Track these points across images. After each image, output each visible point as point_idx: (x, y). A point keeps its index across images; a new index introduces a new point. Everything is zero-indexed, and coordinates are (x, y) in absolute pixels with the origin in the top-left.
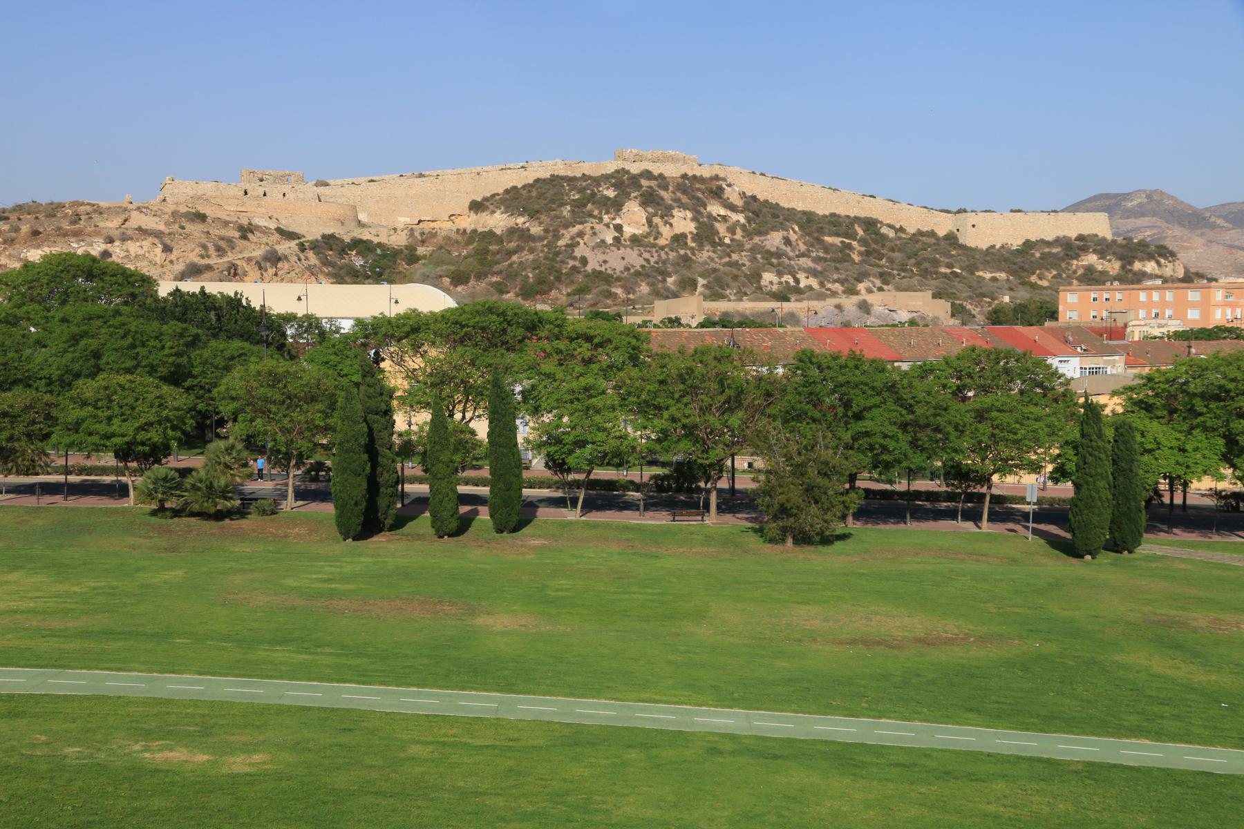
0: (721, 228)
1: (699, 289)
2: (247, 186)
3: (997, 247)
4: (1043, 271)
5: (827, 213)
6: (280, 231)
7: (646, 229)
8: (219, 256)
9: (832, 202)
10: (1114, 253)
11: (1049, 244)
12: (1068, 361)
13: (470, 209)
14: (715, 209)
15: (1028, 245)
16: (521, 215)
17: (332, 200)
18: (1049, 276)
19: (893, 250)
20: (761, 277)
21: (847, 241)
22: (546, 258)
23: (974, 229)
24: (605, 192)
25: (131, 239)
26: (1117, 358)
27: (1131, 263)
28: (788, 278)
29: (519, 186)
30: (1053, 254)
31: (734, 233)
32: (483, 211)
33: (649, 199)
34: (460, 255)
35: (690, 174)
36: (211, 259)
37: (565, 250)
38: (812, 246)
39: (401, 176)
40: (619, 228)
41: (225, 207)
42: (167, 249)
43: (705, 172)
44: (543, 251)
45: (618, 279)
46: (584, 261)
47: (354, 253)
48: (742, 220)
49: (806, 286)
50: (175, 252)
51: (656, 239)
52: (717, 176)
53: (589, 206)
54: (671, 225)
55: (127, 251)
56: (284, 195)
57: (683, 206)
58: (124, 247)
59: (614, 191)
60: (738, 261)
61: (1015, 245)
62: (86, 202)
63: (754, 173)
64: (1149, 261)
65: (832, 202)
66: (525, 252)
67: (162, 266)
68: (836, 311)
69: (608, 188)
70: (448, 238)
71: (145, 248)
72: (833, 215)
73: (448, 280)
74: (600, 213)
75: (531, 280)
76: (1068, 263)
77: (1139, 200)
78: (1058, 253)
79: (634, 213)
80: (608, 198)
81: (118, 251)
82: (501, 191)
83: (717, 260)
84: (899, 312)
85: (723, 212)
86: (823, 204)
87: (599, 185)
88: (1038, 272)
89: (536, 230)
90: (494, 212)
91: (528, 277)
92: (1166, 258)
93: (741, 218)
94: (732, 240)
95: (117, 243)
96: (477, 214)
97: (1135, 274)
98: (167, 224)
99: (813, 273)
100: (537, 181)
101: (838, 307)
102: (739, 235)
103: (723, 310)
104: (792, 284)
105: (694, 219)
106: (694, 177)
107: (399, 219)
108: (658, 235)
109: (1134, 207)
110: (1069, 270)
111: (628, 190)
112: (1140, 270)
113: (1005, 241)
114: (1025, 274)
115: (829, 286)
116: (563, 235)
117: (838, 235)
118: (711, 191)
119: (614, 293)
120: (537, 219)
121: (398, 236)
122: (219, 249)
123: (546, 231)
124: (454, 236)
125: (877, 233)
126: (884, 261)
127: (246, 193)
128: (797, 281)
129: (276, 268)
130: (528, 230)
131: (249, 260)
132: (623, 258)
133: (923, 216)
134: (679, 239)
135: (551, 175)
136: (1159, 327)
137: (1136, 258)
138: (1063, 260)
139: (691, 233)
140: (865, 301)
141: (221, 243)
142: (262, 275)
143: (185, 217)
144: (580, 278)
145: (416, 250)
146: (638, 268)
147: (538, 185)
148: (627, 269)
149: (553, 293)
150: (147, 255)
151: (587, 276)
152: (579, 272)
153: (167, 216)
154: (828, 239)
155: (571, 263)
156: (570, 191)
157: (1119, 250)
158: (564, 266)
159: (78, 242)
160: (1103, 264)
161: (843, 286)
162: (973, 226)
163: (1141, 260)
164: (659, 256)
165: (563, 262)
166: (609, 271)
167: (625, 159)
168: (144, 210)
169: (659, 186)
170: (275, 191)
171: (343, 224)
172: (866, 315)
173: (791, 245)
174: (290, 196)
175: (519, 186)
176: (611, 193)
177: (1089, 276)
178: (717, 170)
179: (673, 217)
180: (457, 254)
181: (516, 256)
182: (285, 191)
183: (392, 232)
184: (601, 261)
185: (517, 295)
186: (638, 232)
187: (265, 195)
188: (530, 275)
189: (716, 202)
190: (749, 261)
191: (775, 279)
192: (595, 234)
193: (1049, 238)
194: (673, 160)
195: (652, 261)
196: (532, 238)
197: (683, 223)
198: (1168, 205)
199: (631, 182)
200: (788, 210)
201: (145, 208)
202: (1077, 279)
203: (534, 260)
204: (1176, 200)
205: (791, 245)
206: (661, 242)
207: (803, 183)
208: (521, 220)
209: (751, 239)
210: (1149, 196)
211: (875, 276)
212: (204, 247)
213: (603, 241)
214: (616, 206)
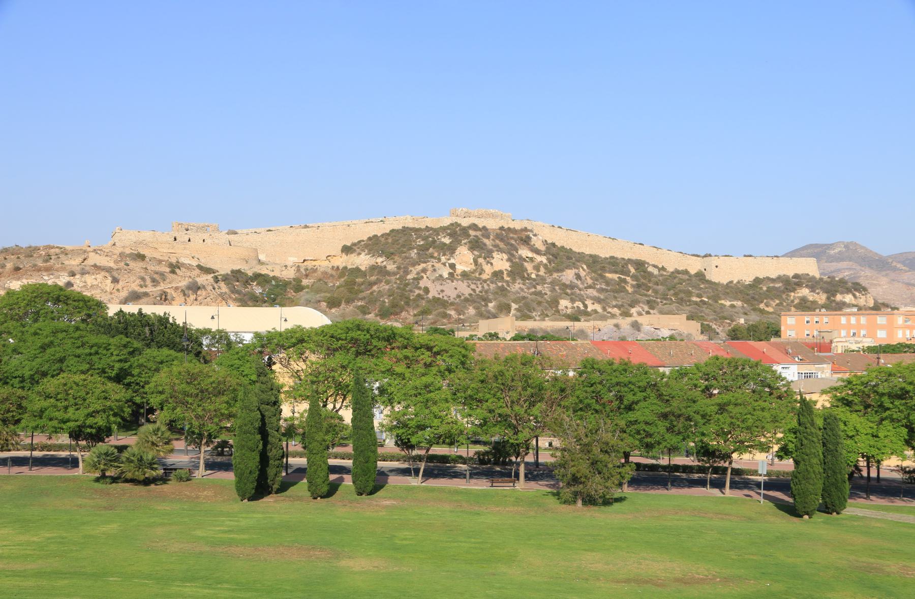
0: (529, 267)
1: (513, 312)
2: (176, 235)
3: (735, 282)
5: (608, 256)
6: (200, 267)
7: (473, 267)
9: (611, 248)
11: (773, 280)
12: (788, 368)
13: (342, 251)
14: (524, 252)
15: (757, 281)
16: (380, 256)
17: (239, 244)
18: (774, 304)
20: (558, 303)
21: (623, 277)
23: (717, 269)
24: (443, 240)
25: (89, 273)
26: (825, 366)
27: (834, 295)
30: (776, 288)
32: (352, 253)
33: (475, 245)
34: (334, 285)
37: (413, 282)
38: (597, 280)
39: (291, 227)
40: (453, 266)
41: (160, 250)
42: (115, 281)
43: (517, 226)
46: (427, 290)
47: (255, 283)
50: (121, 283)
51: (480, 274)
52: (526, 228)
54: (492, 264)
55: (85, 282)
56: (204, 241)
57: (501, 250)
58: (83, 279)
59: (449, 239)
61: (747, 281)
62: (55, 245)
63: (553, 226)
64: (848, 294)
65: (611, 248)
66: (383, 283)
67: (111, 293)
68: (615, 329)
70: (325, 273)
71: (99, 280)
72: (612, 257)
73: (325, 304)
75: (387, 304)
76: (787, 295)
77: (839, 249)
78: (779, 287)
79: (464, 255)
80: (445, 244)
82: (365, 239)
83: (526, 290)
84: (662, 330)
85: (530, 255)
87: (438, 235)
88: (765, 301)
89: (391, 267)
90: (359, 254)
91: (385, 302)
92: (860, 292)
93: (544, 259)
94: (537, 275)
95: (78, 276)
97: (837, 303)
98: (116, 262)
99: (598, 300)
101: (617, 326)
102: (542, 272)
104: (582, 308)
105: (509, 260)
106: (509, 229)
107: (289, 258)
108: (482, 271)
110: (788, 300)
112: (841, 301)
115: (610, 310)
116: (411, 271)
117: (616, 272)
120: (392, 259)
124: (330, 271)
127: (175, 239)
128: (586, 306)
129: (196, 295)
132: (456, 289)
133: (679, 259)
134: (497, 275)
135: (403, 227)
136: (856, 343)
140: (636, 322)
144: (424, 303)
145: (301, 281)
146: (467, 296)
148: (459, 296)
149: (403, 314)
150: (100, 285)
151: (429, 301)
152: (423, 299)
155: (417, 292)
156: (417, 238)
158: (412, 294)
159: (48, 275)
161: (620, 310)
162: (717, 267)
163: (842, 293)
165: (411, 291)
166: (445, 298)
168: (99, 252)
169: (483, 235)
170: (197, 238)
171: (247, 262)
172: (637, 332)
174: (208, 241)
176: (447, 240)
177: (803, 305)
178: (526, 224)
179: (493, 258)
180: (332, 284)
182: (204, 238)
184: (439, 290)
185: (377, 316)
187: (189, 241)
188: (386, 301)
191: (569, 305)
192: (435, 270)
193: (773, 276)
195: (478, 290)
196: (388, 273)
197: (500, 262)
199: (461, 232)
201: (100, 250)
202: (794, 306)
204: (867, 250)
207: (590, 234)
209: (551, 275)
210: (847, 246)
211: (644, 303)
212: (143, 279)
213: (441, 276)
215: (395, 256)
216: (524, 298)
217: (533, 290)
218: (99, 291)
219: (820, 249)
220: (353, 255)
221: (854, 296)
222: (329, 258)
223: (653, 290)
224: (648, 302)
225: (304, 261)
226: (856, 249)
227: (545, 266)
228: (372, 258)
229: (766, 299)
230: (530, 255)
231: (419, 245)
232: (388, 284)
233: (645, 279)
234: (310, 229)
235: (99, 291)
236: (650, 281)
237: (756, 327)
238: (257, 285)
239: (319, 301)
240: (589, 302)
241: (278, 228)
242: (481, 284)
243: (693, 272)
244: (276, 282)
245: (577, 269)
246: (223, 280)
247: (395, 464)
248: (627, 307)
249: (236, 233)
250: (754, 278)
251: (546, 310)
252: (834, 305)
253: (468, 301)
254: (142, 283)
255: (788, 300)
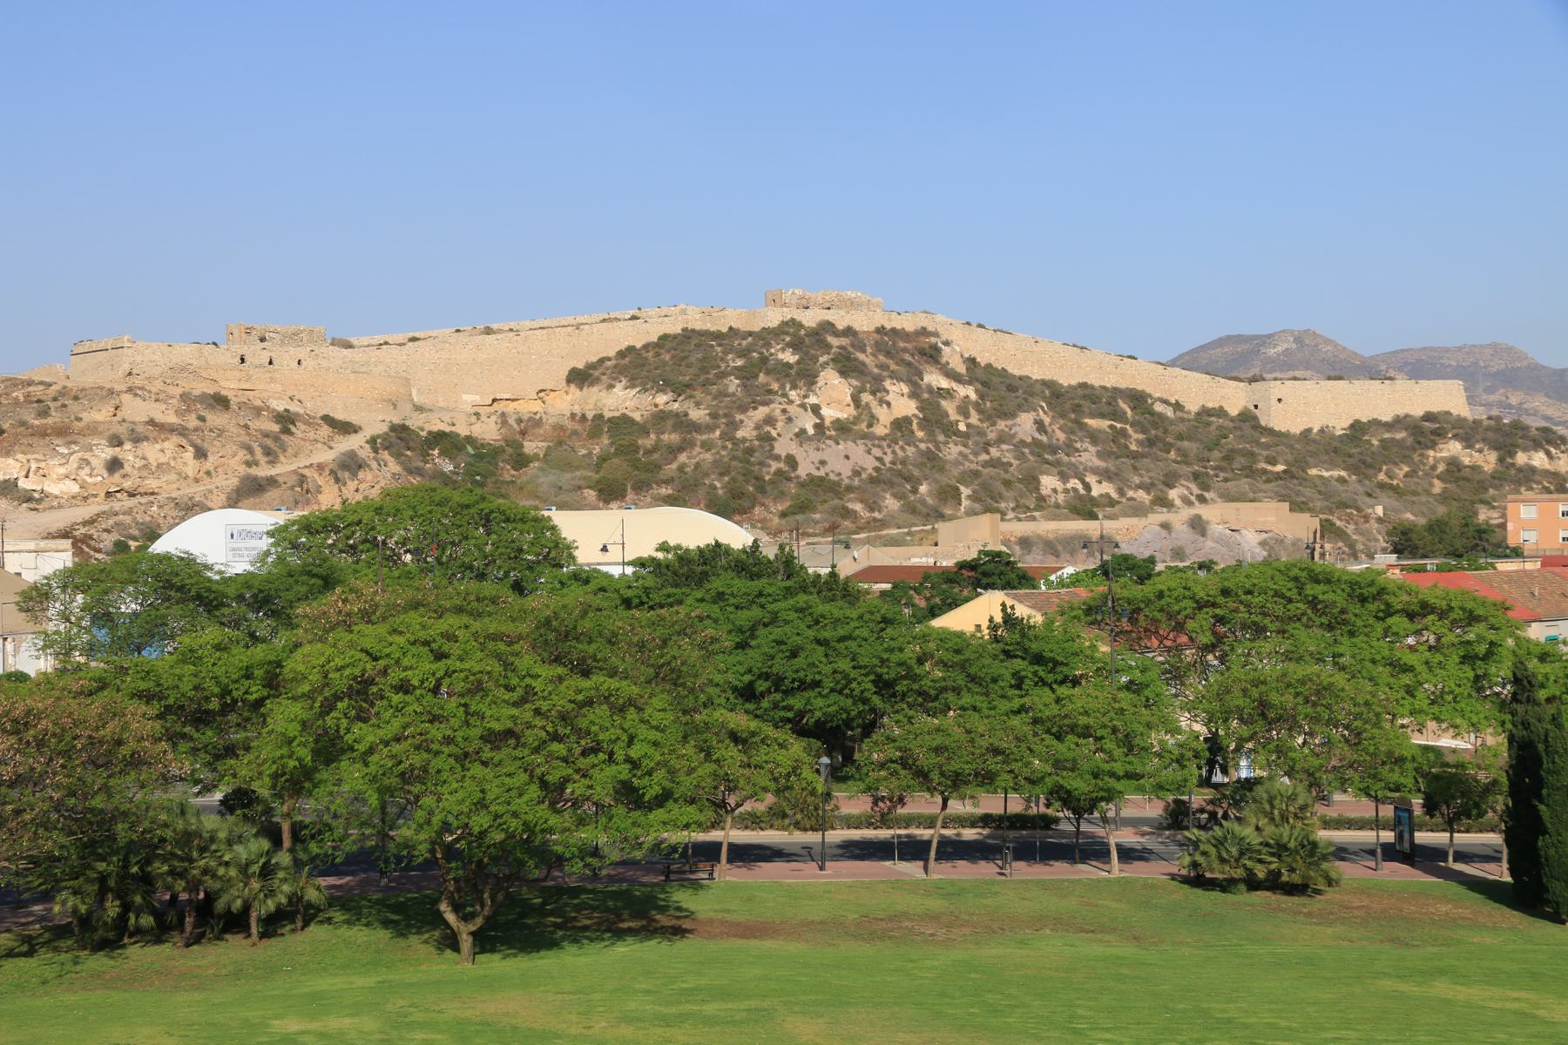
0: (949, 407)
1: (965, 503)
2: (245, 350)
3: (1315, 431)
4: (1391, 466)
5: (1074, 383)
6: (328, 420)
8: (270, 462)
9: (1079, 367)
10: (1484, 440)
11: (1388, 426)
13: (569, 381)
14: (934, 379)
15: (1357, 428)
16: (661, 390)
17: (363, 369)
18: (1401, 474)
19: (1180, 437)
20: (1039, 482)
21: (1119, 426)
22: (734, 458)
23: (1280, 405)
24: (780, 356)
25: (146, 439)
27: (1512, 454)
28: (1074, 483)
29: (638, 346)
30: (1398, 441)
31: (966, 415)
32: (591, 385)
33: (847, 366)
34: (590, 453)
35: (888, 327)
36: (260, 468)
37: (761, 446)
38: (1073, 432)
39: (458, 331)
40: (816, 409)
42: (201, 454)
43: (908, 323)
44: (724, 447)
45: (849, 489)
46: (792, 461)
47: (436, 452)
48: (973, 396)
49: (1101, 495)
50: (211, 458)
51: (870, 425)
52: (924, 329)
53: (762, 378)
54: (889, 404)
55: (144, 458)
56: (299, 362)
57: (895, 376)
58: (139, 453)
59: (793, 354)
60: (999, 458)
61: (1338, 428)
62: (37, 378)
63: (968, 324)
64: (1536, 450)
65: (1079, 367)
66: (698, 449)
68: (1164, 533)
69: (783, 350)
70: (559, 428)
72: (1083, 386)
73: (592, 493)
74: (783, 387)
75: (720, 492)
76: (1422, 455)
77: (1286, 346)
78: (1403, 440)
80: (788, 365)
81: (131, 458)
82: (612, 354)
83: (971, 457)
84: (1244, 532)
85: (944, 383)
86: (1069, 371)
87: (768, 345)
88: (1384, 468)
89: (697, 414)
90: (611, 387)
91: (715, 488)
92: (1557, 447)
93: (970, 392)
94: (968, 426)
95: (128, 446)
96: (581, 389)
97: (1520, 470)
99: (1106, 475)
100: (664, 338)
101: (1166, 526)
102: (974, 419)
103: (1020, 535)
104: (1082, 492)
105: (914, 395)
106: (894, 330)
107: (465, 397)
108: (873, 420)
109: (1278, 355)
110: (1424, 464)
111: (813, 352)
112: (1527, 465)
113: (1324, 422)
114: (1370, 472)
115: (1131, 494)
116: (742, 422)
117: (1102, 416)
118: (922, 353)
119: (852, 510)
120: (691, 397)
121: (484, 426)
122: (268, 452)
123: (714, 416)
124: (569, 425)
125: (1153, 413)
126: (1172, 455)
127: (243, 360)
128: (1087, 487)
130: (686, 415)
131: (320, 467)
132: (847, 457)
134: (901, 425)
137: (1517, 446)
138: (1415, 450)
139: (914, 415)
140: (1198, 517)
141: (269, 442)
142: (340, 490)
143: (201, 403)
144: (792, 488)
145: (522, 446)
146: (870, 471)
147: (668, 345)
148: (857, 473)
149: (757, 510)
150: (172, 464)
151: (802, 485)
152: (789, 479)
153: (174, 401)
154: (1091, 422)
155: (775, 466)
156: (725, 353)
157: (1490, 434)
158: (764, 470)
159: (68, 444)
160: (1471, 456)
161: (1149, 493)
162: (1280, 400)
163: (1525, 450)
164: (894, 452)
165: (762, 464)
166: (832, 477)
167: (784, 305)
168: (139, 392)
169: (853, 345)
170: (286, 357)
173: (1046, 432)
174: (309, 363)
175: (638, 346)
176: (789, 357)
177: (1457, 474)
178: (921, 321)
179: (888, 392)
180: (584, 452)
181: (684, 454)
183: (474, 419)
184: (816, 462)
186: (843, 415)
187: (271, 363)
188: (718, 485)
189: (933, 369)
190: (1015, 458)
191: (1059, 486)
192: (790, 420)
193: (1386, 417)
194: (852, 305)
195: (888, 459)
196: (696, 427)
197: (899, 402)
198: (1326, 352)
199: (813, 340)
200: (1021, 378)
202: (1438, 477)
203: (715, 462)
204: (1336, 345)
205: (1046, 432)
206: (880, 430)
207: (1038, 339)
208: (662, 399)
209: (994, 424)
210: (1299, 340)
211: (1187, 479)
212: (250, 449)
213: (803, 431)
214: (806, 376)
215: (694, 390)
216: (976, 474)
217: (984, 457)
218: (173, 476)
219: (1247, 346)
220: (595, 389)
221: (1548, 454)
222: (542, 395)
223: (1179, 450)
224: (1196, 477)
225: (494, 400)
226: (1316, 345)
227: (977, 405)
228: (643, 396)
229: (1385, 463)
230: (944, 383)
231: (736, 368)
232: (709, 450)
233: (1157, 429)
234: (499, 336)
235: (173, 476)
236: (1166, 431)
237: (1446, 524)
238: (440, 455)
239: (580, 488)
240: (1091, 479)
241: (430, 333)
242: (889, 446)
243: (1234, 411)
244: (475, 448)
245: (1035, 410)
246: (386, 448)
247: (1367, 836)
248: (1161, 487)
249: (350, 346)
250: (1350, 421)
251: (1022, 497)
252: (1513, 472)
253: (879, 480)
254: (248, 457)
255: (1424, 464)
